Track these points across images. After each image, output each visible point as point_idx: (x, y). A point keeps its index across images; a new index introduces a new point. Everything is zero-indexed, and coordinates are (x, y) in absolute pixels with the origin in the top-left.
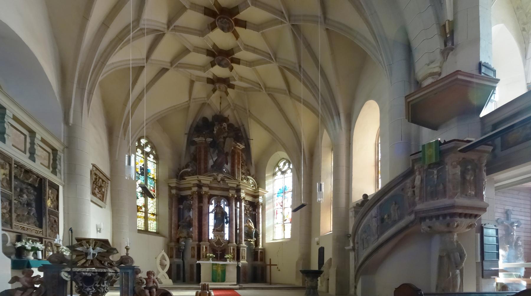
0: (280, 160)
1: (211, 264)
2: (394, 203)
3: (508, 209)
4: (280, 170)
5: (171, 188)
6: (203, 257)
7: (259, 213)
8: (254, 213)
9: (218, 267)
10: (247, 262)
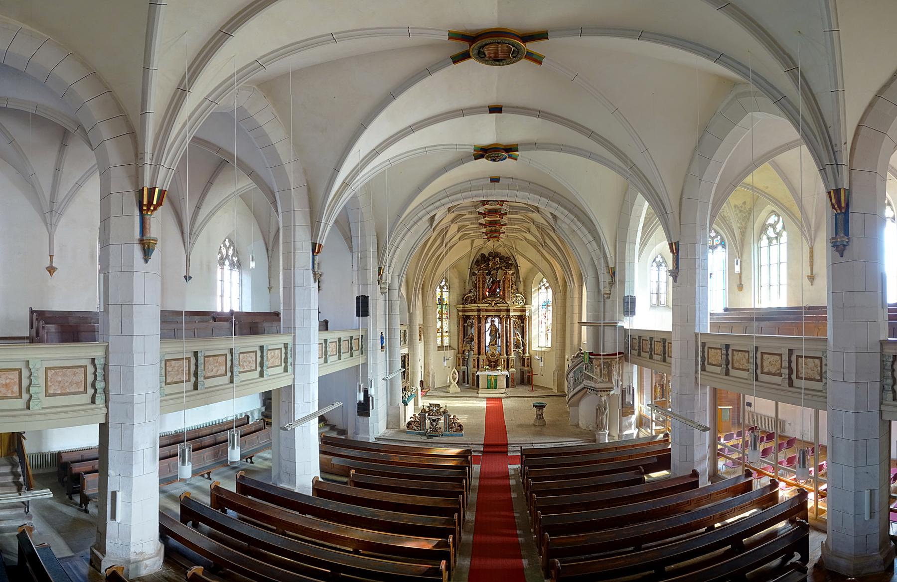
5: (459, 311)
8: (522, 325)
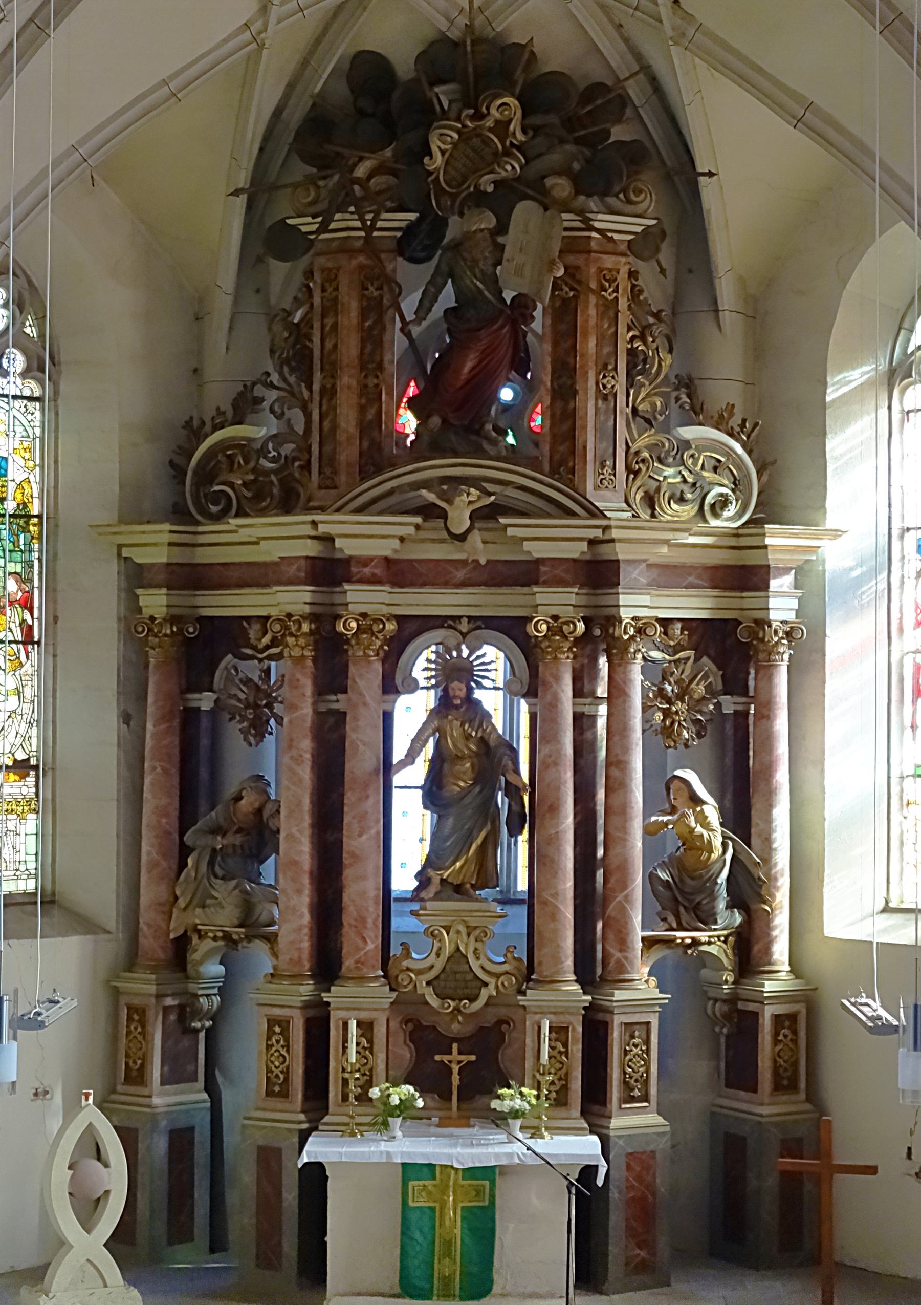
1: (400, 1169)
6: (345, 1098)
7: (766, 713)
8: (729, 704)
9: (444, 1190)
10: (661, 1120)
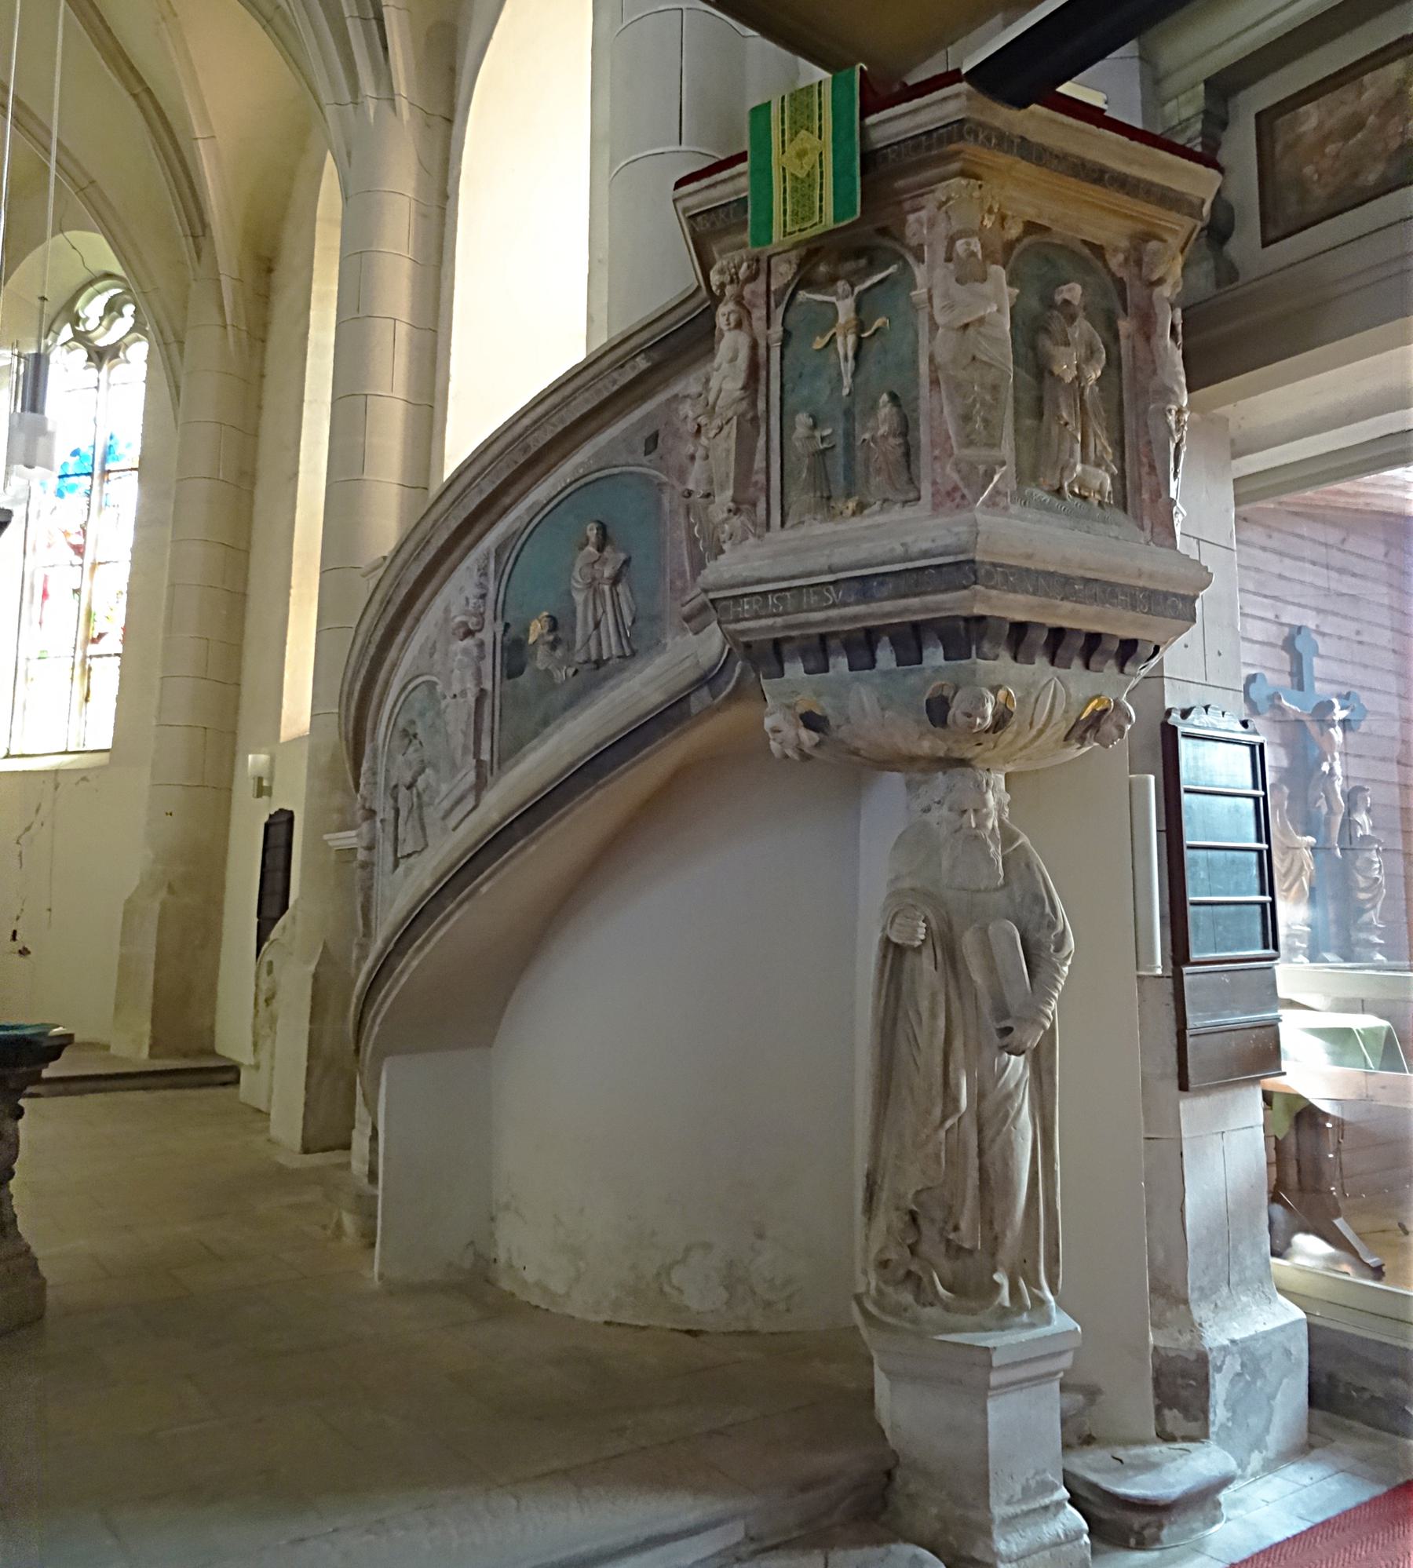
0: (91, 283)
2: (592, 532)
3: (1298, 623)
4: (81, 338)
